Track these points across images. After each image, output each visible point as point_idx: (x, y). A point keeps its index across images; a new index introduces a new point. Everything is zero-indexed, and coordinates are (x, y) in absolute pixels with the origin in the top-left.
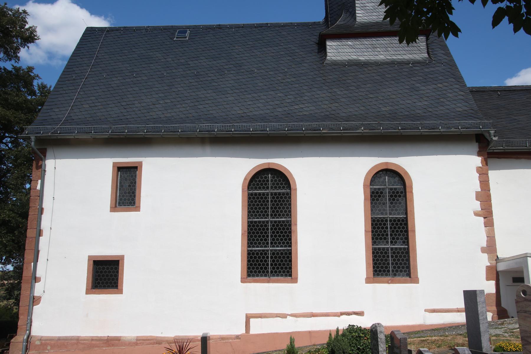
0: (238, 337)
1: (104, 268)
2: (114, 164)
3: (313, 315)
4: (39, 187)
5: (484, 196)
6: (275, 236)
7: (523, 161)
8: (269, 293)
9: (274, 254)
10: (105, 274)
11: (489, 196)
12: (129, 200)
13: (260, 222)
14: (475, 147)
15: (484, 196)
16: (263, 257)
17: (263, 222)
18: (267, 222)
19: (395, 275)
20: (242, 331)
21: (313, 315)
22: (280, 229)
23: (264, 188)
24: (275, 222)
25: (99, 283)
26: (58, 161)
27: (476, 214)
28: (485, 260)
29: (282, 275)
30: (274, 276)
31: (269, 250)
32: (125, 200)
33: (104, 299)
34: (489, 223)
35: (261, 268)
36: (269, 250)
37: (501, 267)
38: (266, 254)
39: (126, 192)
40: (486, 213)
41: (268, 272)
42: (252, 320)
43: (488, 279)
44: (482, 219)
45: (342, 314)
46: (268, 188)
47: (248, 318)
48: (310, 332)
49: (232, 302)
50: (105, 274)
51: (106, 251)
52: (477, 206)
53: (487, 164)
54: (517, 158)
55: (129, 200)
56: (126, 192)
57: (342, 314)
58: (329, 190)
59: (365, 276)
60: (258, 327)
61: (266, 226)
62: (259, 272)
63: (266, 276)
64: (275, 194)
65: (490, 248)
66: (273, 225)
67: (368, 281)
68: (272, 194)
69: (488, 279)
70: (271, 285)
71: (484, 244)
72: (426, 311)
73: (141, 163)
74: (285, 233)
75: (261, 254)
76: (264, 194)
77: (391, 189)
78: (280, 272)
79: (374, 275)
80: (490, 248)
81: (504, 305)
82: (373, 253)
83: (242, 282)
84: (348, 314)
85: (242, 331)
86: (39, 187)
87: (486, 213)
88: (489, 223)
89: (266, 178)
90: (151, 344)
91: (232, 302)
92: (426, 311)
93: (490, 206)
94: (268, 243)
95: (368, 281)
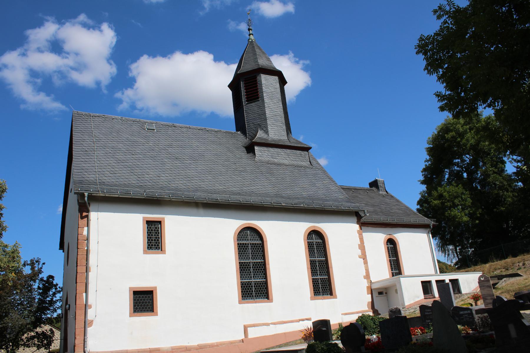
1: (140, 297)
2: (143, 218)
4: (85, 233)
5: (362, 247)
6: (255, 272)
7: (370, 228)
8: (256, 309)
9: (255, 284)
10: (144, 301)
11: (364, 247)
12: (155, 245)
13: (245, 263)
14: (355, 219)
15: (362, 247)
16: (249, 287)
17: (247, 263)
18: (250, 263)
19: (323, 294)
20: (242, 337)
22: (257, 267)
23: (245, 240)
24: (255, 262)
25: (137, 308)
26: (99, 213)
28: (365, 284)
29: (262, 298)
30: (257, 298)
31: (254, 283)
32: (152, 245)
33: (144, 320)
34: (366, 263)
35: (249, 294)
36: (254, 283)
37: (374, 287)
38: (250, 284)
39: (154, 239)
40: (364, 256)
41: (253, 296)
42: (249, 329)
43: (368, 294)
46: (248, 240)
47: (246, 328)
48: (285, 333)
49: (235, 319)
50: (144, 301)
52: (359, 252)
53: (361, 229)
54: (368, 226)
55: (155, 245)
56: (154, 239)
58: (285, 241)
59: (310, 296)
60: (253, 333)
61: (249, 265)
62: (248, 296)
63: (252, 299)
64: (253, 244)
65: (367, 276)
66: (253, 265)
67: (312, 299)
68: (248, 240)
69: (368, 294)
70: (257, 304)
71: (365, 274)
72: (342, 314)
73: (164, 218)
74: (262, 268)
75: (248, 284)
76: (246, 244)
77: (316, 242)
78: (260, 296)
79: (315, 295)
80: (367, 276)
81: (376, 308)
82: (313, 281)
83: (239, 303)
84: (303, 320)
85: (242, 337)
86: (85, 233)
87: (364, 256)
88: (366, 263)
89: (246, 233)
90: (183, 351)
91: (235, 319)
92: (342, 314)
93: (365, 252)
94: (251, 277)
95: (312, 299)
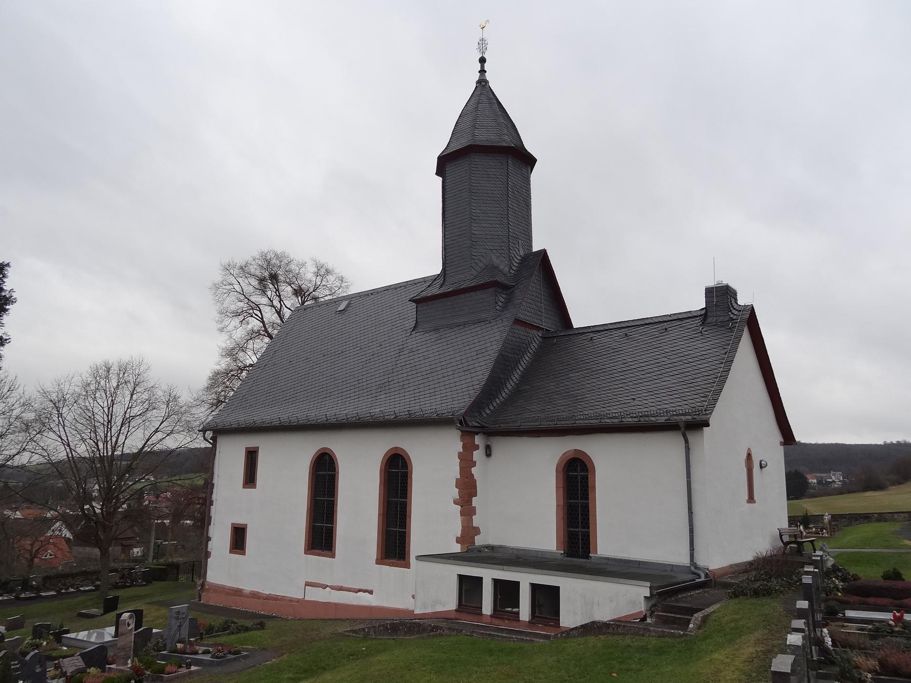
0: (298, 601)
3: (341, 589)
21: (341, 589)
27: (455, 503)
42: (479, 541)
44: (459, 508)
45: (360, 591)
48: (336, 604)
51: (240, 521)
57: (360, 591)
95: (379, 561)
